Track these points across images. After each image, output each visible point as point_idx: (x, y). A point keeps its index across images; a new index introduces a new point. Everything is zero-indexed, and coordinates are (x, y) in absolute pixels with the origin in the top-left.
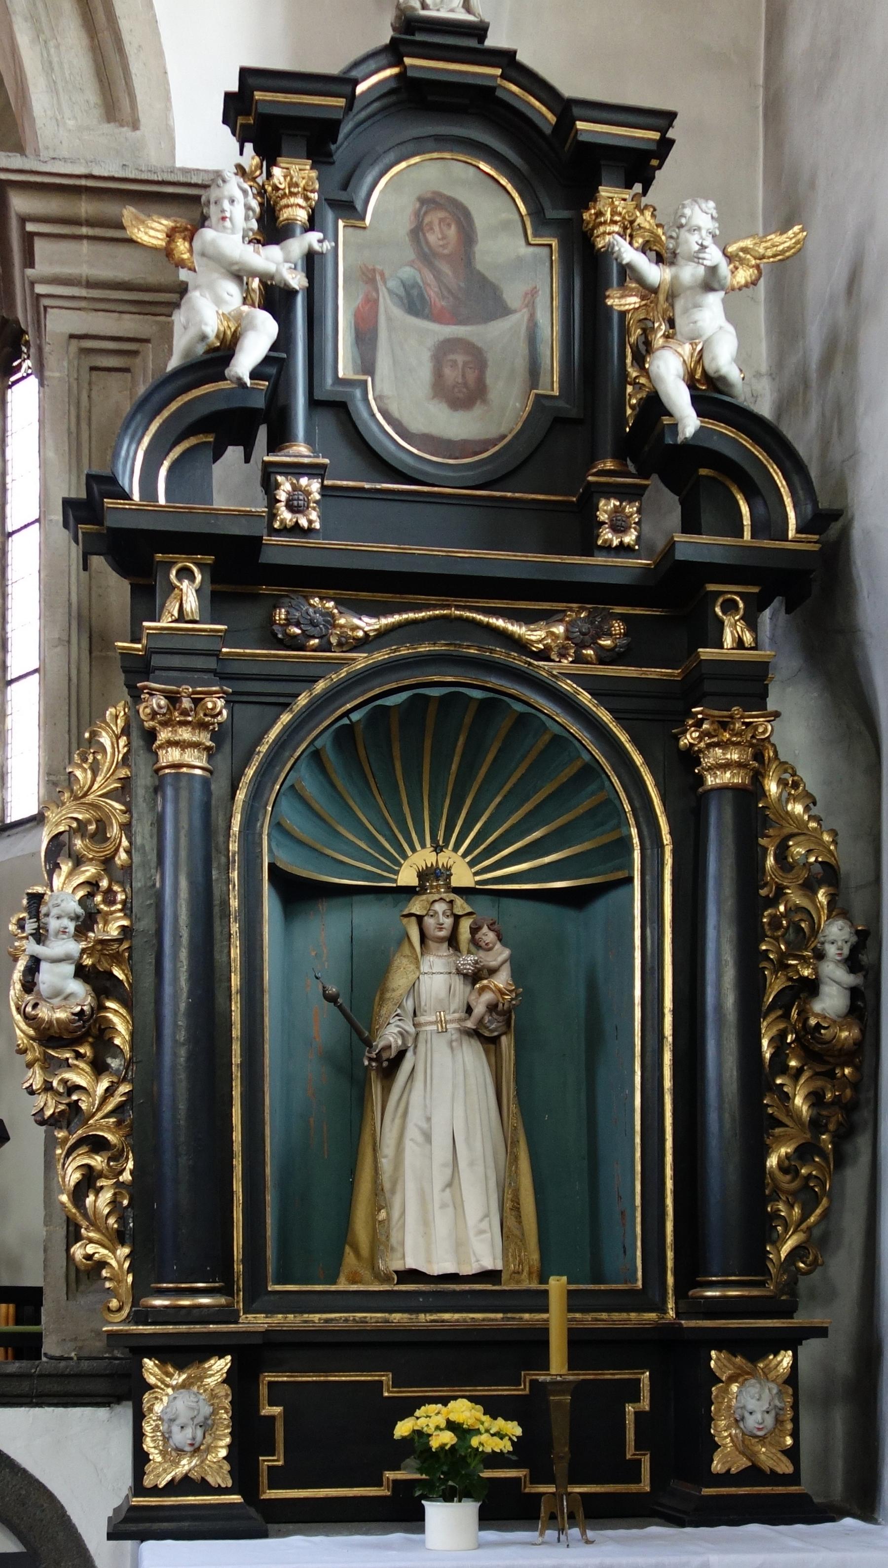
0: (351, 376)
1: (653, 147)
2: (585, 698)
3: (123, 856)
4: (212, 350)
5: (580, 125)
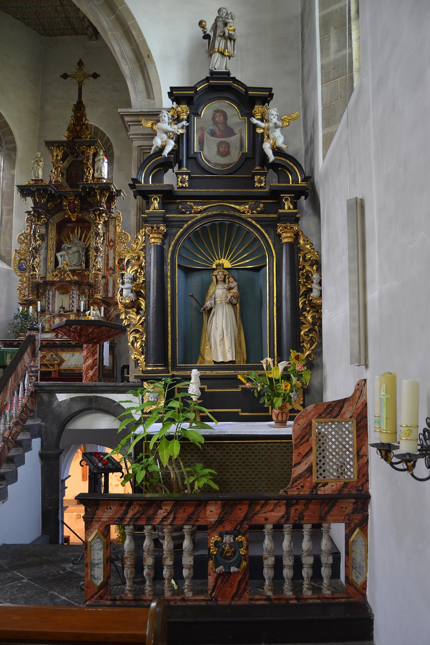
0: (198, 151)
1: (267, 96)
2: (254, 222)
3: (144, 264)
4: (160, 149)
5: (249, 92)
